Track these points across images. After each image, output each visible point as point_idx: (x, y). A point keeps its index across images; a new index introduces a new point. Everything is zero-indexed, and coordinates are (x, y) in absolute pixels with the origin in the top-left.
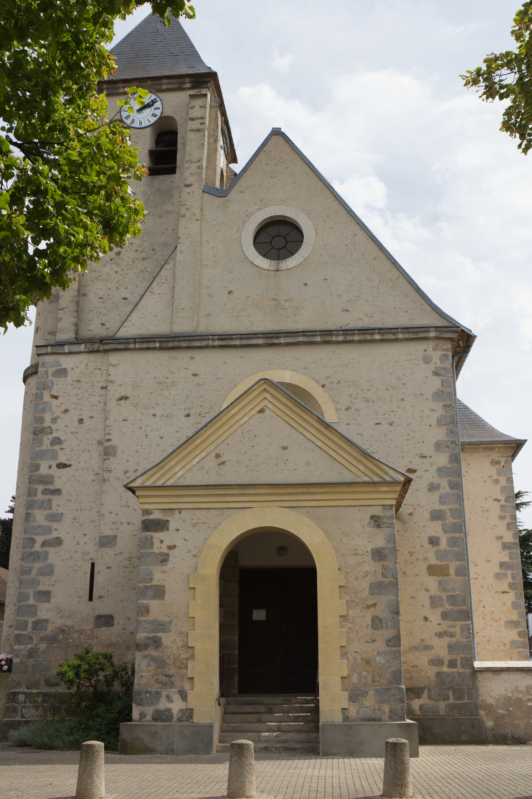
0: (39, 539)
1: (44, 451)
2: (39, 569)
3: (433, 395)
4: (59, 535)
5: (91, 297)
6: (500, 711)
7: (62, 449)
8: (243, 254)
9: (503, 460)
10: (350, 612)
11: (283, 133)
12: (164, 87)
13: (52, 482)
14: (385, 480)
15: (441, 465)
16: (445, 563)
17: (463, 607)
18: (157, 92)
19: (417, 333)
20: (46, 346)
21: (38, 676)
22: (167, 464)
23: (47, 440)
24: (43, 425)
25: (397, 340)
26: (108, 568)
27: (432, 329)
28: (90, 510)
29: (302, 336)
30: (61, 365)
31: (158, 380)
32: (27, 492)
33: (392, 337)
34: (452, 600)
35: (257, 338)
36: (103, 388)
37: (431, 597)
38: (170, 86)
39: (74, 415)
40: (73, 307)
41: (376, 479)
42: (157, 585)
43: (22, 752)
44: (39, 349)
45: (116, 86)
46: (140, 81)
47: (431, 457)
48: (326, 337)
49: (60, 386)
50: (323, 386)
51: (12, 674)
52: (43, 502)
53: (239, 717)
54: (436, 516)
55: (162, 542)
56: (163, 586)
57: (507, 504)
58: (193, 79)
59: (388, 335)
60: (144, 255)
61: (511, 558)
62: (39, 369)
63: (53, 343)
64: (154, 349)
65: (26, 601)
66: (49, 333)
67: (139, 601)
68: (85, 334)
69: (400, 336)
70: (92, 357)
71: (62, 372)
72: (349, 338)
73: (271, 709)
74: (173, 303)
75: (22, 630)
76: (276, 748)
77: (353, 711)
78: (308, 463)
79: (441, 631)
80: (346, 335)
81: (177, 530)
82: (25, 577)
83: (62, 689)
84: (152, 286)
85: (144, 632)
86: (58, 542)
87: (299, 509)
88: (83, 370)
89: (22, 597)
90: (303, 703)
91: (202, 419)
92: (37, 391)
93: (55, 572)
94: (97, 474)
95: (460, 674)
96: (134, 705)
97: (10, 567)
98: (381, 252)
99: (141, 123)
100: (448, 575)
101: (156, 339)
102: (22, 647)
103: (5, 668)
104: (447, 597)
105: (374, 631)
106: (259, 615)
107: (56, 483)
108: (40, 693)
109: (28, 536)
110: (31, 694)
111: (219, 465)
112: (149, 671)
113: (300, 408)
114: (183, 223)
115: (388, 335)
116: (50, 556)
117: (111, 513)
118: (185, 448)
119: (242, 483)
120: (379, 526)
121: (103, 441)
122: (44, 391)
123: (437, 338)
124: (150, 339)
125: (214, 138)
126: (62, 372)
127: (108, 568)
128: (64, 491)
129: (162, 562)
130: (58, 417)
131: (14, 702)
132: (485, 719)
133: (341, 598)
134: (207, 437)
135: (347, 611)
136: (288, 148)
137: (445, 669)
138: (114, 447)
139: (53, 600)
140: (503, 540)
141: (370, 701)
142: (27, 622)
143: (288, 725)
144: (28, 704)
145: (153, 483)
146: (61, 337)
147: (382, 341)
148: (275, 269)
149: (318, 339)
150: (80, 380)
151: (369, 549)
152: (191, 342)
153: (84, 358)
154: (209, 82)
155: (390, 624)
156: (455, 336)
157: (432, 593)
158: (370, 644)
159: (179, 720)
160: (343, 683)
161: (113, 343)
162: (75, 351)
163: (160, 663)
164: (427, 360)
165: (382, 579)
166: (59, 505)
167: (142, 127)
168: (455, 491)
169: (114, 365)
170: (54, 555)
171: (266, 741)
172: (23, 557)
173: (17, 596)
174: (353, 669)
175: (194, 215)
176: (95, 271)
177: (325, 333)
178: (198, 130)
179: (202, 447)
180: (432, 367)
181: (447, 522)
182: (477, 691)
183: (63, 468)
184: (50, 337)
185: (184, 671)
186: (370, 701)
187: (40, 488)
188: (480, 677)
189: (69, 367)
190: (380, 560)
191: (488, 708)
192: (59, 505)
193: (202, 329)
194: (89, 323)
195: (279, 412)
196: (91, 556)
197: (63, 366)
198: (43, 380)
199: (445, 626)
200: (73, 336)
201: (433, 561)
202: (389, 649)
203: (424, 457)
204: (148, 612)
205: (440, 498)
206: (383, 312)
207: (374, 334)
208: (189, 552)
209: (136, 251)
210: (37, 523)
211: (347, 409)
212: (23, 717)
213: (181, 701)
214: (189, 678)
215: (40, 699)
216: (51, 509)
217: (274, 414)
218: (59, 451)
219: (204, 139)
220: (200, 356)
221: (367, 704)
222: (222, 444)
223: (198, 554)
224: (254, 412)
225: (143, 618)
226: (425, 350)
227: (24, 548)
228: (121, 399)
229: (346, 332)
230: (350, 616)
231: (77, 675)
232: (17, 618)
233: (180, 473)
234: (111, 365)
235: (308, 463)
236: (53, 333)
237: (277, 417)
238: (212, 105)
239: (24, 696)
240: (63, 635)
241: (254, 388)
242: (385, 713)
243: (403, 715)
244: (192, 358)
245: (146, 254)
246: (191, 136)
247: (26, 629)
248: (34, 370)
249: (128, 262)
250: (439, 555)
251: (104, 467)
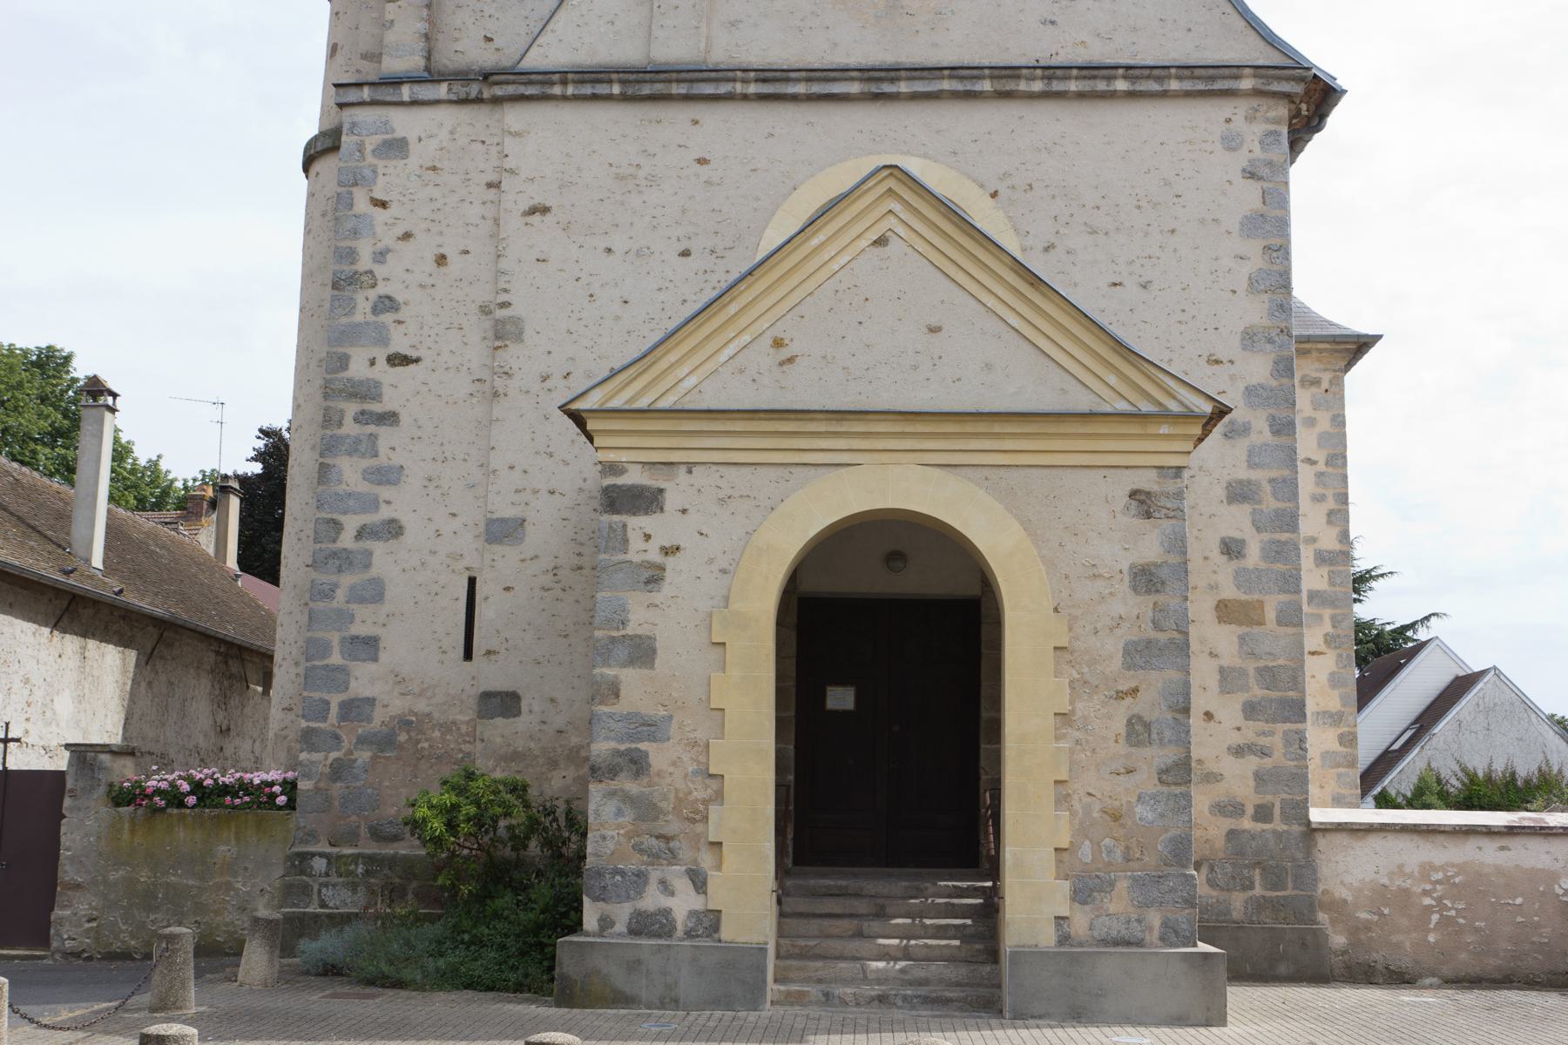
0: (351, 523)
1: (358, 325)
2: (352, 588)
3: (1242, 224)
4: (395, 515)
6: (1363, 915)
7: (400, 322)
9: (1326, 377)
10: (1079, 705)
13: (377, 397)
14: (1167, 409)
15: (1254, 381)
16: (1256, 596)
17: (1291, 693)
19: (1213, 79)
20: (359, 85)
21: (354, 818)
23: (364, 302)
24: (354, 267)
25: (1164, 95)
26: (507, 589)
27: (1247, 71)
29: (951, 77)
30: (393, 131)
32: (321, 419)
33: (1154, 86)
34: (1268, 676)
36: (490, 185)
37: (1222, 670)
39: (424, 247)
41: (1146, 407)
42: (636, 636)
43: (334, 996)
44: (341, 90)
47: (1231, 362)
48: (1002, 83)
49: (391, 178)
50: (994, 195)
51: (297, 814)
52: (358, 441)
53: (814, 925)
54: (1239, 493)
55: (648, 537)
56: (652, 639)
57: (1330, 470)
59: (1144, 82)
61: (1332, 583)
62: (344, 138)
63: (373, 78)
64: (609, 98)
65: (324, 657)
66: (364, 57)
67: (597, 671)
69: (1174, 85)
71: (396, 147)
72: (1057, 86)
73: (883, 907)
75: (316, 719)
76: (905, 998)
77: (1080, 923)
79: (1241, 742)
80: (1050, 78)
81: (684, 511)
83: (409, 848)
85: (607, 738)
86: (393, 529)
87: (964, 470)
89: (314, 649)
90: (949, 896)
93: (388, 595)
95: (1278, 835)
96: (585, 899)
97: (282, 581)
100: (1261, 623)
101: (614, 76)
102: (316, 756)
103: (282, 800)
104: (1258, 669)
105: (1133, 750)
106: (841, 698)
107: (385, 398)
108: (359, 855)
109: (324, 515)
110: (339, 857)
111: (781, 364)
112: (619, 826)
113: (972, 237)
115: (1144, 82)
116: (377, 559)
117: (512, 468)
120: (1148, 515)
122: (354, 190)
123: (1257, 93)
126: (396, 147)
127: (507, 589)
128: (405, 418)
129: (647, 582)
130: (388, 250)
131: (302, 873)
132: (1329, 931)
133: (1057, 674)
135: (1071, 703)
137: (1247, 824)
138: (517, 321)
139: (383, 656)
140: (1318, 546)
141: (1118, 903)
142: (328, 703)
143: (926, 946)
144: (334, 879)
146: (394, 65)
147: (1131, 95)
149: (986, 86)
151: (1125, 567)
153: (447, 116)
155: (1168, 734)
156: (1298, 89)
157: (1225, 662)
158: (1121, 778)
159: (689, 934)
160: (1059, 862)
161: (514, 83)
163: (646, 810)
164: (1231, 143)
165: (1153, 634)
168: (1283, 440)
169: (517, 134)
171: (879, 981)
172: (315, 561)
173: (300, 643)
174: (1083, 830)
177: (1004, 72)
179: (743, 321)
180: (1241, 159)
181: (1263, 507)
182: (1315, 871)
183: (401, 365)
184: (366, 66)
185: (699, 828)
186: (1118, 903)
187: (351, 408)
188: (1322, 842)
189: (412, 137)
190: (1148, 592)
191: (1337, 907)
193: (720, 55)
194: (456, 34)
196: (466, 563)
197: (399, 134)
199: (1250, 732)
201: (1229, 592)
202: (1165, 789)
203: (1218, 362)
204: (617, 696)
205: (1251, 453)
206: (1135, 29)
207: (1115, 78)
208: (711, 561)
210: (344, 486)
211: (1047, 249)
212: (323, 905)
213: (692, 892)
214: (712, 844)
215: (360, 870)
218: (392, 326)
220: (715, 119)
221: (1112, 908)
224: (864, 243)
225: (605, 709)
226: (1228, 121)
227: (316, 541)
228: (532, 211)
230: (1079, 714)
231: (451, 826)
232: (305, 694)
233: (690, 380)
235: (988, 367)
236: (374, 57)
239: (324, 861)
240: (408, 732)
241: (864, 187)
242: (1151, 929)
243: (1193, 934)
244: (696, 122)
247: (325, 719)
248: (328, 143)
250: (1242, 578)
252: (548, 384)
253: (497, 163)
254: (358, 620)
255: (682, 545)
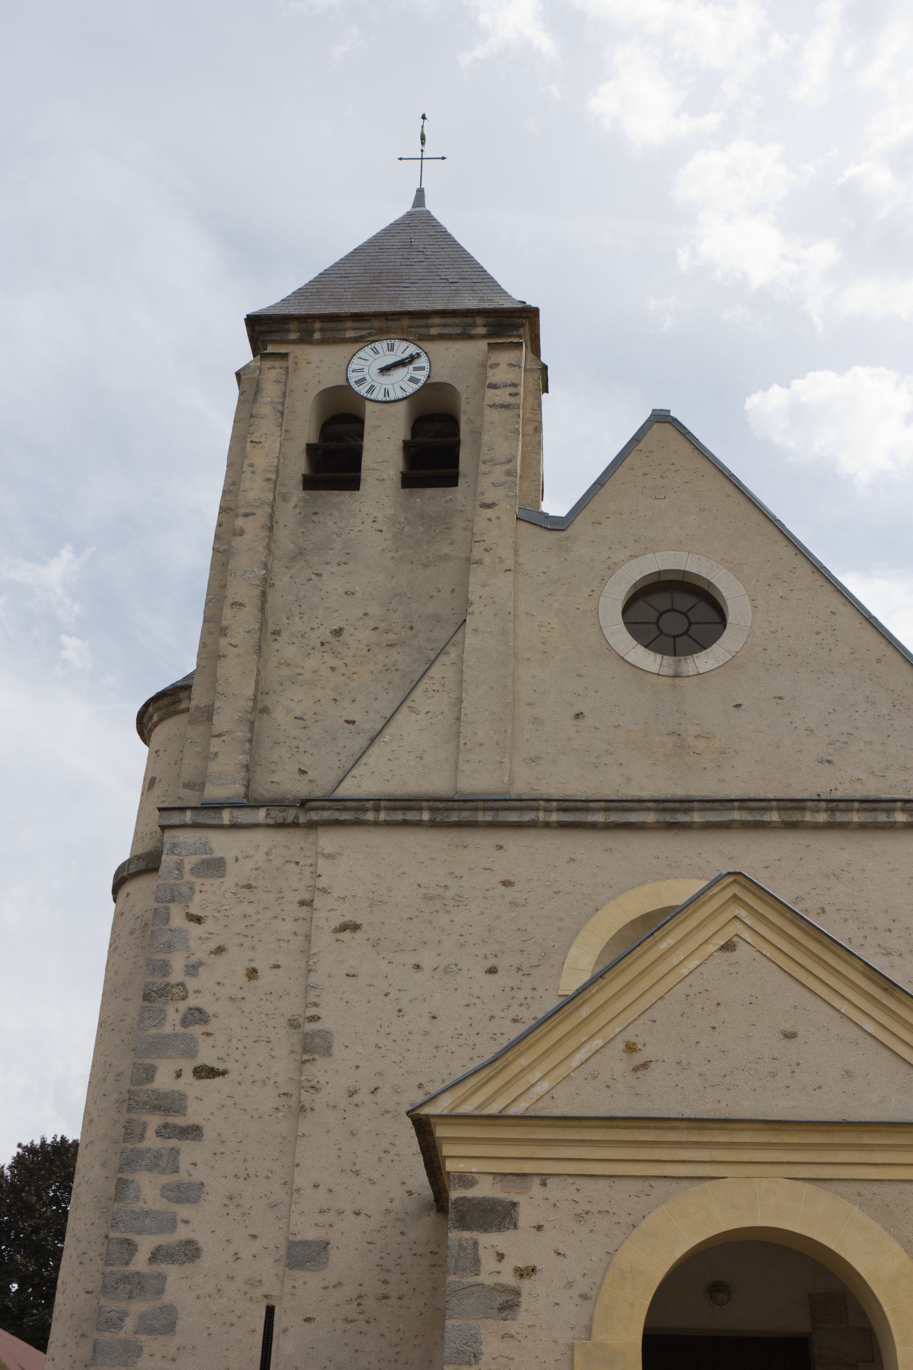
0: (146, 1244)
2: (142, 1317)
4: (192, 1236)
5: (280, 716)
7: (208, 1034)
8: (603, 642)
11: (675, 420)
12: (434, 331)
13: (181, 1110)
18: (419, 340)
20: (182, 809)
22: (511, 1062)
23: (173, 1014)
24: (166, 979)
26: (308, 1320)
28: (268, 1177)
30: (212, 851)
31: (426, 891)
35: (642, 810)
36: (302, 903)
38: (446, 331)
40: (242, 733)
44: (165, 814)
45: (340, 325)
46: (387, 320)
49: (207, 895)
52: (158, 1155)
55: (501, 1257)
58: (491, 320)
60: (391, 637)
62: (164, 857)
64: (419, 824)
66: (186, 785)
68: (262, 791)
70: (280, 837)
71: (214, 867)
74: (458, 734)
78: (847, 1073)
80: (833, 810)
81: (539, 1228)
82: (107, 1336)
84: (414, 696)
86: (190, 1252)
88: (260, 864)
91: (524, 978)
92: (157, 905)
93: (181, 1325)
94: (284, 1094)
98: (891, 648)
99: (386, 393)
101: (424, 804)
107: (190, 1111)
111: (635, 1069)
114: (477, 576)
117: (316, 1186)
118: (554, 1027)
119: (693, 1116)
121: (300, 1020)
122: (171, 905)
124: (411, 804)
125: (535, 424)
126: (214, 867)
127: (308, 1320)
128: (208, 1132)
129: (502, 1309)
134: (605, 1003)
136: (687, 448)
138: (326, 1036)
145: (477, 1108)
146: (215, 792)
148: (671, 672)
149: (774, 817)
150: (254, 884)
152: (500, 813)
153: (263, 838)
154: (522, 326)
161: (329, 809)
162: (244, 822)
166: (195, 1164)
167: (388, 399)
170: (179, 1284)
175: (501, 560)
176: (289, 665)
177: (790, 804)
178: (506, 406)
179: (594, 1026)
187: (154, 1121)
189: (229, 857)
192: (195, 1164)
193: (521, 788)
195: (769, 952)
196: (264, 1290)
197: (217, 854)
198: (172, 882)
200: (241, 790)
207: (894, 810)
209: (375, 629)
210: (141, 1204)
216: (177, 1172)
217: (758, 955)
219: (518, 422)
222: (641, 1020)
223: (593, 1293)
224: (711, 948)
228: (343, 928)
229: (835, 804)
233: (538, 1086)
234: (323, 855)
235: (849, 1074)
236: (198, 786)
237: (766, 961)
238: (528, 367)
244: (500, 848)
245: (396, 637)
246: (492, 415)
248: (141, 866)
249: (357, 649)
251: (303, 1078)
252: (356, 1099)
253: (311, 883)
254: (146, 1352)
255: (538, 1267)
